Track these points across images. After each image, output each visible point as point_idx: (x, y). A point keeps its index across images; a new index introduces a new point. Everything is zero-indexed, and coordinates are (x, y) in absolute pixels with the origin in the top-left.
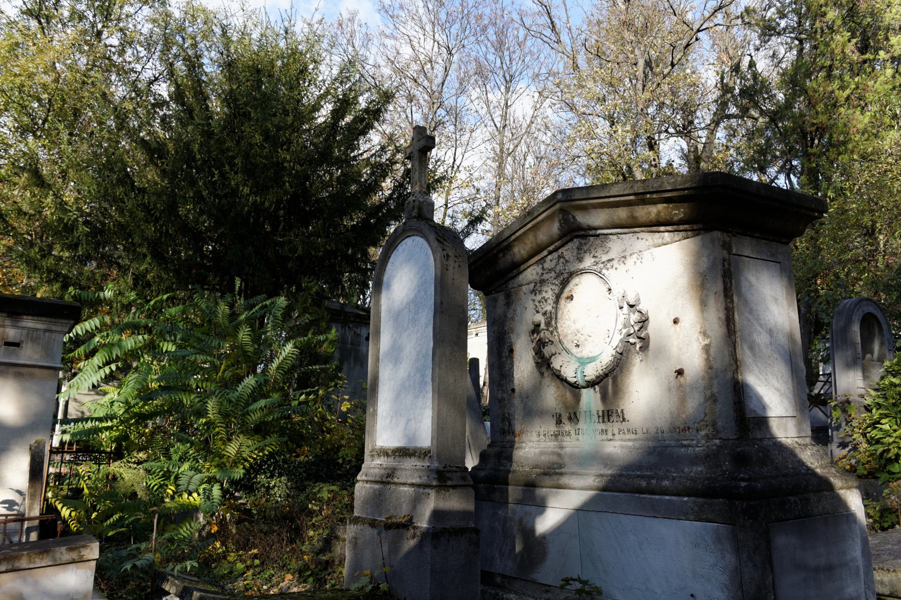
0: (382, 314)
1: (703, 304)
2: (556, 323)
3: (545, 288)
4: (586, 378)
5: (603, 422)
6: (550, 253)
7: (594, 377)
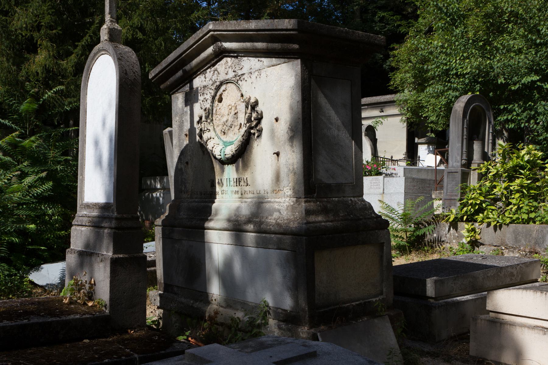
2: (212, 117)
3: (206, 92)
4: (227, 156)
6: (209, 67)
7: (230, 155)
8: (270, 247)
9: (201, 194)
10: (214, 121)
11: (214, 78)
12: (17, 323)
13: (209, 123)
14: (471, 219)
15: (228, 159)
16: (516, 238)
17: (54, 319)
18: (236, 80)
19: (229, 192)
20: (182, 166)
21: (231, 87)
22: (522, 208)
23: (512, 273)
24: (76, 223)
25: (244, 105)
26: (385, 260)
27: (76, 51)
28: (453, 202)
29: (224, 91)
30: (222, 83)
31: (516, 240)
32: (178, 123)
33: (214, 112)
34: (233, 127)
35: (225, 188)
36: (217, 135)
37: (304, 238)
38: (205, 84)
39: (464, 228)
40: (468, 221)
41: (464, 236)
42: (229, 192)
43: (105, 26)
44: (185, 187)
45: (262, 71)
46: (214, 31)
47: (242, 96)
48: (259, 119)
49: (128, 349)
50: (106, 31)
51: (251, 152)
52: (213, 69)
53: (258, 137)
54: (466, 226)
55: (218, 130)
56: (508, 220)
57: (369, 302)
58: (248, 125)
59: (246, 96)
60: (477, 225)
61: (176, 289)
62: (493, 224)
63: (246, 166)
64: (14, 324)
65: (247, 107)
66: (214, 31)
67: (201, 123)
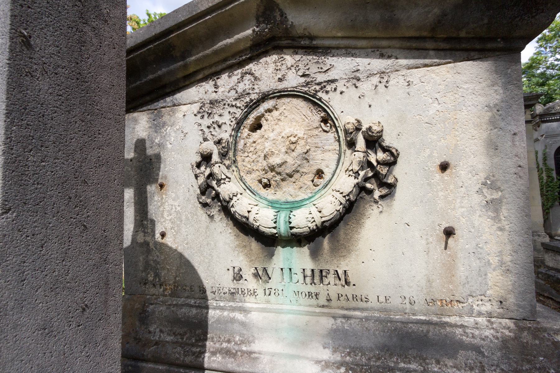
0: (550, 123)
1: (493, 147)
2: (235, 156)
4: (294, 230)
5: (313, 283)
10: (240, 164)
29: (269, 111)
30: (265, 97)
33: (240, 146)
44: (157, 275)
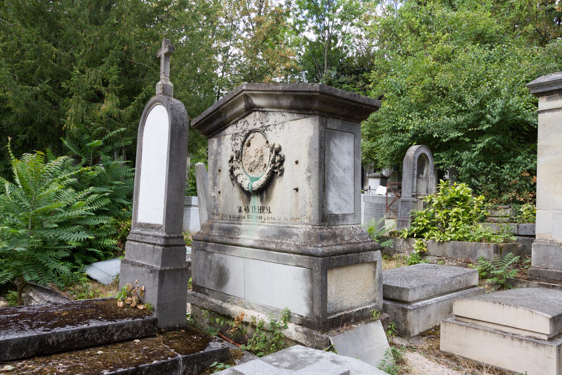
3: (237, 138)
6: (241, 119)
8: (290, 264)
9: (230, 217)
10: (243, 161)
11: (244, 127)
12: (78, 328)
13: (239, 163)
14: (420, 235)
15: (254, 191)
16: (454, 251)
17: (110, 323)
18: (263, 130)
19: (254, 217)
20: (215, 195)
21: (258, 135)
22: (458, 229)
23: (460, 281)
24: (130, 238)
25: (268, 150)
26: (377, 274)
27: (133, 103)
28: (405, 223)
29: (252, 138)
30: (250, 132)
31: (454, 253)
32: (213, 161)
33: (243, 154)
34: (259, 166)
35: (250, 213)
36: (245, 172)
37: (320, 259)
38: (236, 131)
39: (414, 243)
40: (417, 237)
41: (414, 249)
42: (254, 217)
43: (160, 83)
44: (217, 211)
45: (285, 124)
46: (247, 90)
47: (267, 142)
48: (282, 161)
49: (172, 349)
50: (161, 87)
51: (274, 186)
52: (243, 120)
53: (280, 175)
54: (416, 241)
55: (246, 168)
56: (449, 239)
57: (366, 309)
58: (272, 165)
59: (271, 143)
60: (424, 240)
61: (207, 291)
62: (437, 241)
63: (268, 198)
64: (75, 328)
65: (272, 151)
66: (247, 90)
67: (232, 162)
